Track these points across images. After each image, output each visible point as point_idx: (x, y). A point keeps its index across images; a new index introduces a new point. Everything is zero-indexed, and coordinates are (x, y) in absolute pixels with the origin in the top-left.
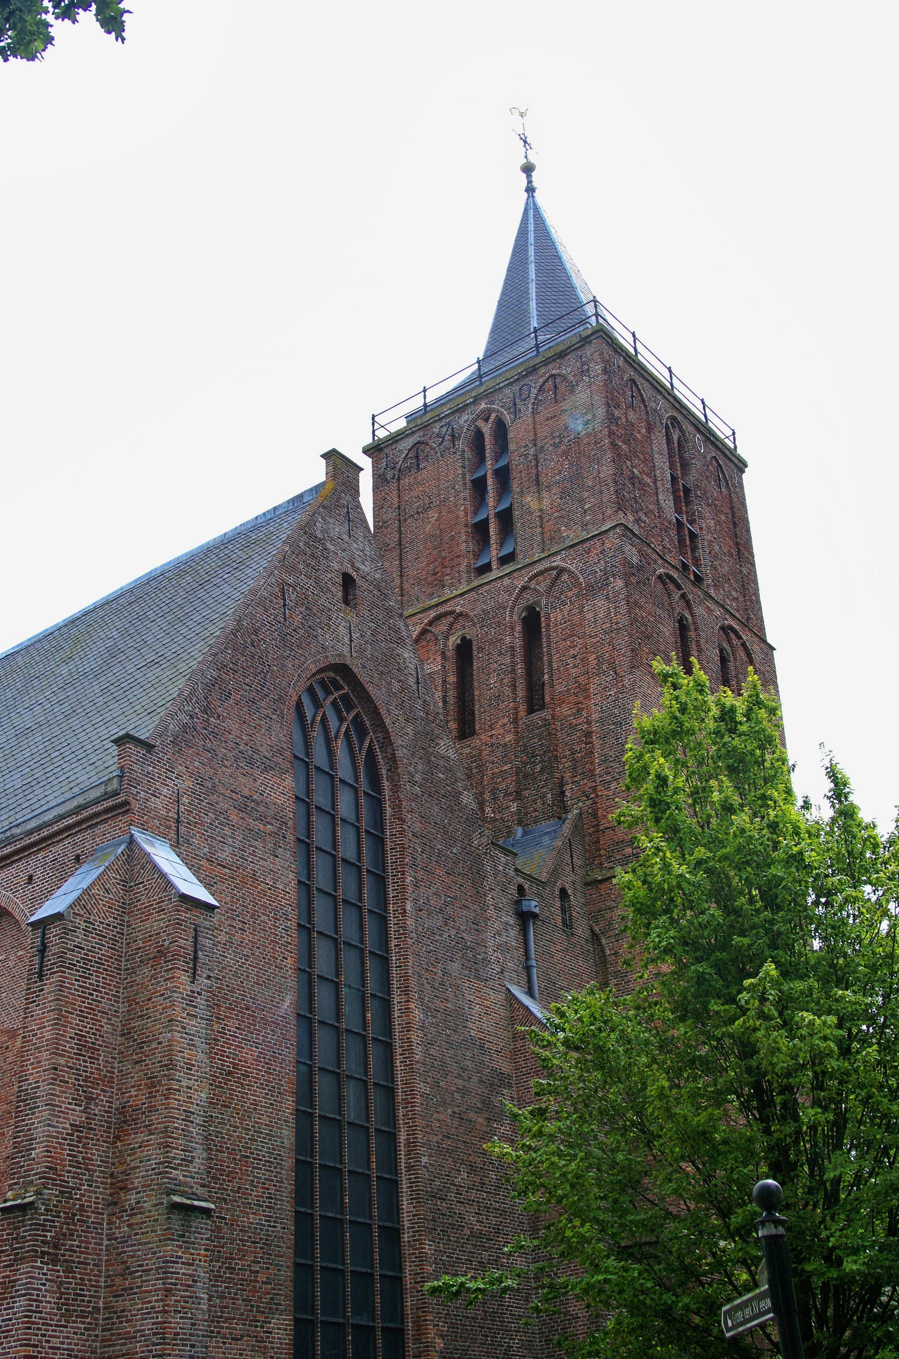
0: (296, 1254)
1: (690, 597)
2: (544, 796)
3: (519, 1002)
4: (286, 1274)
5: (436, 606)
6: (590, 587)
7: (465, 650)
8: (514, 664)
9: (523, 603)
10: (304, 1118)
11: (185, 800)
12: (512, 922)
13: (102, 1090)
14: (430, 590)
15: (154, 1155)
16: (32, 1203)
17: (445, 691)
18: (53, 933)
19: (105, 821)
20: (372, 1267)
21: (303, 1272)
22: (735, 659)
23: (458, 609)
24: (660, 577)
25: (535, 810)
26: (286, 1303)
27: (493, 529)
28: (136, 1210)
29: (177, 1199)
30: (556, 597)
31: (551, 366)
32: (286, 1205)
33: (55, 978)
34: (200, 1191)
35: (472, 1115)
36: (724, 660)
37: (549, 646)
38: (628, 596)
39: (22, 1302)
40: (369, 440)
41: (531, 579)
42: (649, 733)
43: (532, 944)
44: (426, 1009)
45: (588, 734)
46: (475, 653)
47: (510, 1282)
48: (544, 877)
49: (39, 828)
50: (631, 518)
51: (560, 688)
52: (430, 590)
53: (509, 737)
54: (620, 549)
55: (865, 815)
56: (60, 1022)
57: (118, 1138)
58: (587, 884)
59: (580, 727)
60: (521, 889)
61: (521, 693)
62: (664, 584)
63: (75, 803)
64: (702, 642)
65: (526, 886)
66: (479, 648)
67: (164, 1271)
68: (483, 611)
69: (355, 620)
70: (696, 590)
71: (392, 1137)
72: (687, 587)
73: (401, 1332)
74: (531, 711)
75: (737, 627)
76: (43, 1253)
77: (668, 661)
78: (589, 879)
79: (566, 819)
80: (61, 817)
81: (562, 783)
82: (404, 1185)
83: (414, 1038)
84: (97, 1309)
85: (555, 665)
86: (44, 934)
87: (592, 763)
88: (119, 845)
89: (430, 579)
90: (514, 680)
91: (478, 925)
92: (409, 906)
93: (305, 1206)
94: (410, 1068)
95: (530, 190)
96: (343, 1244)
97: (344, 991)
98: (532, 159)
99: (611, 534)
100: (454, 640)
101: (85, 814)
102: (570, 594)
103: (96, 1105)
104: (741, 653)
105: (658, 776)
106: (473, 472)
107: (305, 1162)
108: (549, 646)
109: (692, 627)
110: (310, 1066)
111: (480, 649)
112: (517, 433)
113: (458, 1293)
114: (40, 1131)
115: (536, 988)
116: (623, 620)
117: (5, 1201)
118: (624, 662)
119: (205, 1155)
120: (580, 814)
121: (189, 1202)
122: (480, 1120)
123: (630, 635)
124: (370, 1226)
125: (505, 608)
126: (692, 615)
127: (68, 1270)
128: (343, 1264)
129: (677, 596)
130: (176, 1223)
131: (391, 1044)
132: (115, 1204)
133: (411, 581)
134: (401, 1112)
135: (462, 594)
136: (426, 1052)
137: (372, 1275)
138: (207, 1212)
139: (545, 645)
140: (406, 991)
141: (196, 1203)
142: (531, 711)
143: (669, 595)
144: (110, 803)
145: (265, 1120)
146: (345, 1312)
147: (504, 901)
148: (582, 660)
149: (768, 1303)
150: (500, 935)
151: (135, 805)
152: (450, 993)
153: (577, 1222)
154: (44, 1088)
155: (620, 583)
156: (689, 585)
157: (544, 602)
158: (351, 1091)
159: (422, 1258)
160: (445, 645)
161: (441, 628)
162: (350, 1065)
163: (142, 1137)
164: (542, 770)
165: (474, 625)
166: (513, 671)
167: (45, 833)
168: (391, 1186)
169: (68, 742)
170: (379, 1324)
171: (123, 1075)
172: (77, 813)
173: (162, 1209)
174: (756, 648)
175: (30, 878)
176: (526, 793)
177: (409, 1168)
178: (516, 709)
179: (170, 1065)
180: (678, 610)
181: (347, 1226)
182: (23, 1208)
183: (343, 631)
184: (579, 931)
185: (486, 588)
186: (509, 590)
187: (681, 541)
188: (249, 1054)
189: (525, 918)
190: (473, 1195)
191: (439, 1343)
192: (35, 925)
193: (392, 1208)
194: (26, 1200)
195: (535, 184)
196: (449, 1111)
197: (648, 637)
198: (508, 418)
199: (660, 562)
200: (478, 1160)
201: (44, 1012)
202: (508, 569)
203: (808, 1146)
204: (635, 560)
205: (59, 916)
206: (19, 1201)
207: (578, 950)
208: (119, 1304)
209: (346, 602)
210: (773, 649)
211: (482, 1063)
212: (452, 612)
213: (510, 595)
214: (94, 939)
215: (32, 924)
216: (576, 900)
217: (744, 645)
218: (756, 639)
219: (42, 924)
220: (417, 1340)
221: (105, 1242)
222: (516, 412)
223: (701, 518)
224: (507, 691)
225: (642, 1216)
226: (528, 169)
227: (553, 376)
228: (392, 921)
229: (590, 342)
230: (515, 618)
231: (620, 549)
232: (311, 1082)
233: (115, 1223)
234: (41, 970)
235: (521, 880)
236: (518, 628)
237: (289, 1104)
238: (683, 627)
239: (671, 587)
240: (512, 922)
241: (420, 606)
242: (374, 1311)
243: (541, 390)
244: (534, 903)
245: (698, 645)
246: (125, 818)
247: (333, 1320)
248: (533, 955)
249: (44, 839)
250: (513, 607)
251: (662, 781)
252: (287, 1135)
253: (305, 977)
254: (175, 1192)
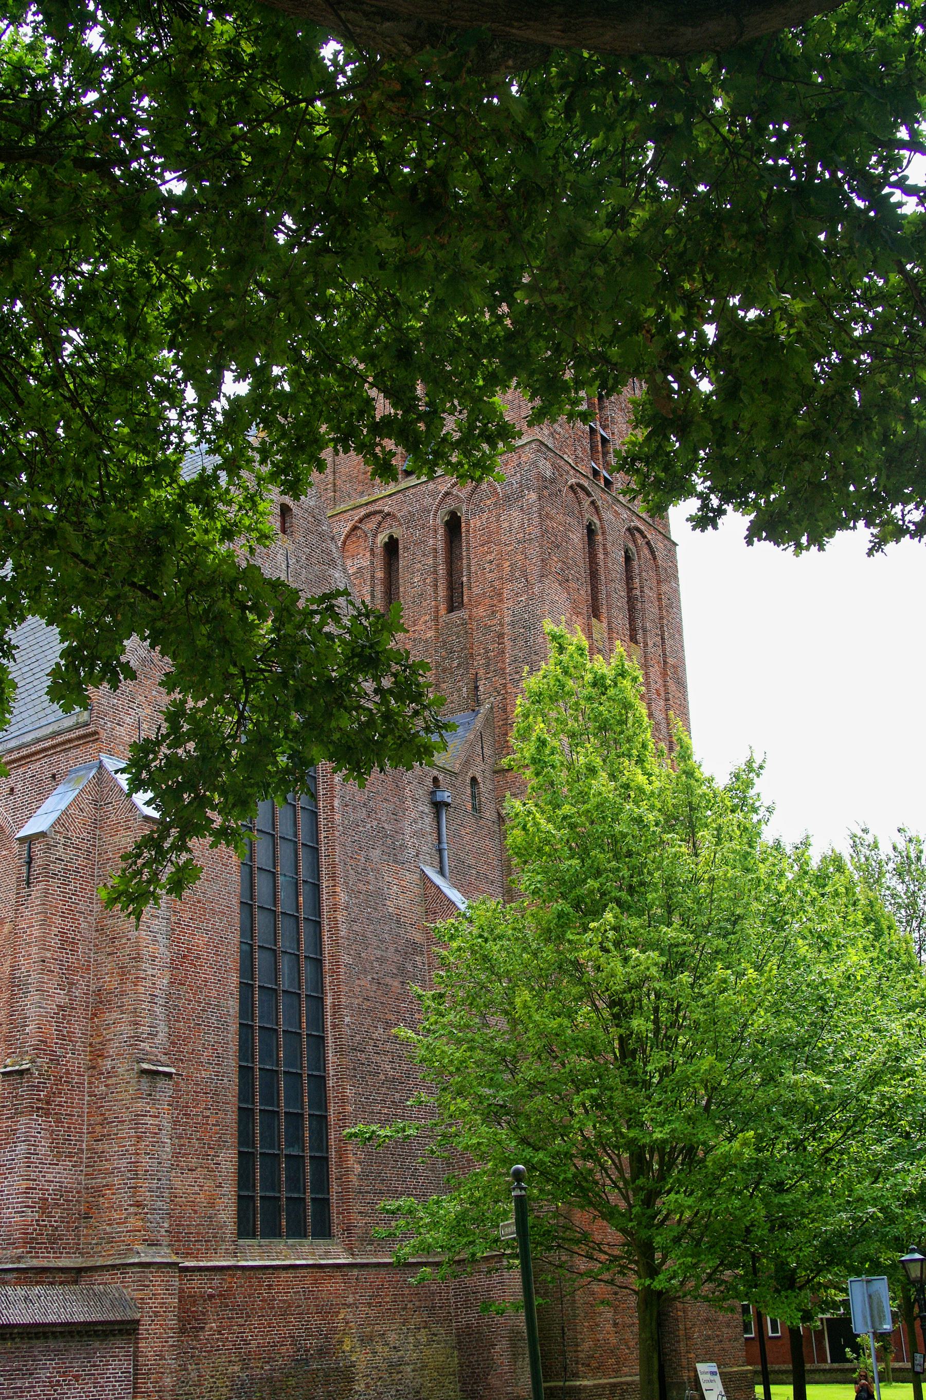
0: (240, 1101)
1: (599, 503)
2: (459, 690)
3: (431, 882)
4: (231, 1117)
5: (366, 504)
6: (507, 498)
7: (392, 547)
8: (436, 566)
9: (446, 508)
10: (246, 989)
11: (145, 726)
12: (427, 811)
13: (82, 977)
14: (360, 488)
15: (126, 1030)
16: (28, 1069)
17: (373, 587)
18: (38, 847)
19: (77, 746)
20: (302, 1109)
21: (245, 1115)
22: (639, 558)
23: (387, 509)
24: (571, 487)
25: (452, 702)
26: (231, 1139)
28: (110, 1074)
29: (145, 1066)
30: (476, 505)
32: (232, 1063)
33: (41, 886)
34: (163, 1058)
35: (388, 980)
36: (628, 559)
37: (468, 550)
38: (541, 508)
39: (22, 1147)
42: (535, 694)
43: (444, 830)
44: (350, 892)
45: (501, 635)
46: (401, 552)
47: (411, 1132)
48: (457, 768)
49: (19, 748)
50: (546, 432)
51: (476, 591)
52: (360, 488)
53: (431, 634)
54: (535, 464)
55: (705, 772)
56: (46, 922)
57: (95, 1015)
58: (495, 772)
59: (493, 628)
60: (435, 780)
61: (442, 592)
62: (575, 493)
63: (50, 729)
64: (609, 545)
65: (440, 778)
66: (404, 547)
67: (137, 1122)
69: (291, 547)
70: (605, 496)
71: (319, 1001)
72: (597, 494)
73: (326, 1159)
74: (451, 609)
75: (642, 528)
76: (38, 1108)
77: (557, 623)
78: (497, 768)
79: (478, 712)
80: (39, 740)
81: (476, 679)
82: (330, 1040)
83: (339, 918)
84: (82, 1150)
85: (473, 569)
86: (30, 848)
87: (504, 662)
88: (91, 769)
89: (361, 477)
90: (436, 580)
91: (396, 816)
92: (336, 803)
93: (247, 1061)
94: (336, 943)
96: (278, 1090)
97: (280, 879)
99: (527, 448)
100: (382, 538)
101: (60, 739)
102: (489, 502)
103: (77, 988)
104: (646, 552)
105: (539, 739)
107: (247, 1025)
108: (468, 550)
109: (600, 532)
110: (251, 945)
111: (406, 549)
113: (369, 1139)
114: (32, 1012)
115: (447, 868)
116: (536, 532)
117: (6, 1067)
118: (534, 571)
119: (167, 1030)
120: (492, 708)
121: (154, 1068)
122: (396, 984)
123: (541, 546)
124: (301, 1075)
125: (429, 511)
126: (600, 520)
127: (58, 1121)
128: (279, 1106)
129: (586, 503)
130: (145, 1083)
131: (319, 923)
132: (94, 1068)
133: (344, 478)
134: (328, 980)
135: (390, 495)
136: (350, 929)
137: (302, 1115)
138: (169, 1075)
139: (464, 549)
140: (333, 877)
141: (161, 1069)
142: (451, 609)
143: (580, 503)
144: (81, 732)
145: (214, 993)
146: (279, 1145)
147: (421, 792)
148: (497, 565)
149: (514, 1228)
150: (416, 823)
151: (103, 735)
152: (371, 876)
153: (459, 1100)
154: (34, 977)
155: (533, 496)
156: (599, 491)
157: (464, 508)
158: (285, 964)
159: (343, 1101)
160: (374, 543)
161: (370, 525)
162: (283, 943)
163: (115, 1015)
164: (459, 665)
165: (401, 525)
166: (435, 572)
167: (24, 752)
168: (319, 1041)
169: (37, 657)
170: (308, 1153)
171: (98, 964)
172: (52, 738)
173: (133, 1074)
174: (659, 545)
175: (12, 789)
176: (444, 686)
177: (334, 1026)
179: (138, 958)
180: (587, 516)
181: (282, 1076)
182: (21, 1073)
183: (280, 558)
184: (487, 815)
185: (412, 491)
186: (433, 494)
187: (593, 448)
188: (200, 940)
189: (438, 806)
190: (388, 1047)
191: (358, 1169)
192: (22, 840)
193: (319, 1060)
194: (24, 1067)
196: (369, 978)
197: (558, 547)
199: (572, 472)
200: (393, 1018)
201: (31, 916)
204: (548, 474)
205: (43, 834)
206: (17, 1068)
207: (485, 831)
208: (100, 1147)
209: (284, 531)
210: (675, 544)
211: (398, 935)
212: (380, 512)
214: (71, 852)
215: (18, 839)
216: (484, 787)
217: (648, 543)
218: (660, 537)
219: (29, 840)
220: (339, 1166)
221: (87, 1098)
223: (613, 422)
224: (430, 590)
225: (511, 1092)
228: (322, 816)
230: (438, 521)
231: (535, 464)
232: (252, 959)
233: (93, 1083)
234: (28, 879)
235: (435, 773)
236: (441, 531)
237: (234, 979)
238: (591, 531)
239: (582, 495)
240: (427, 811)
241: (352, 503)
242: (303, 1143)
244: (447, 794)
245: (605, 549)
246: (95, 746)
247: (271, 1151)
249: (28, 756)
250: (436, 511)
251: (543, 743)
252: (233, 1005)
253: (247, 869)
254: (143, 1060)
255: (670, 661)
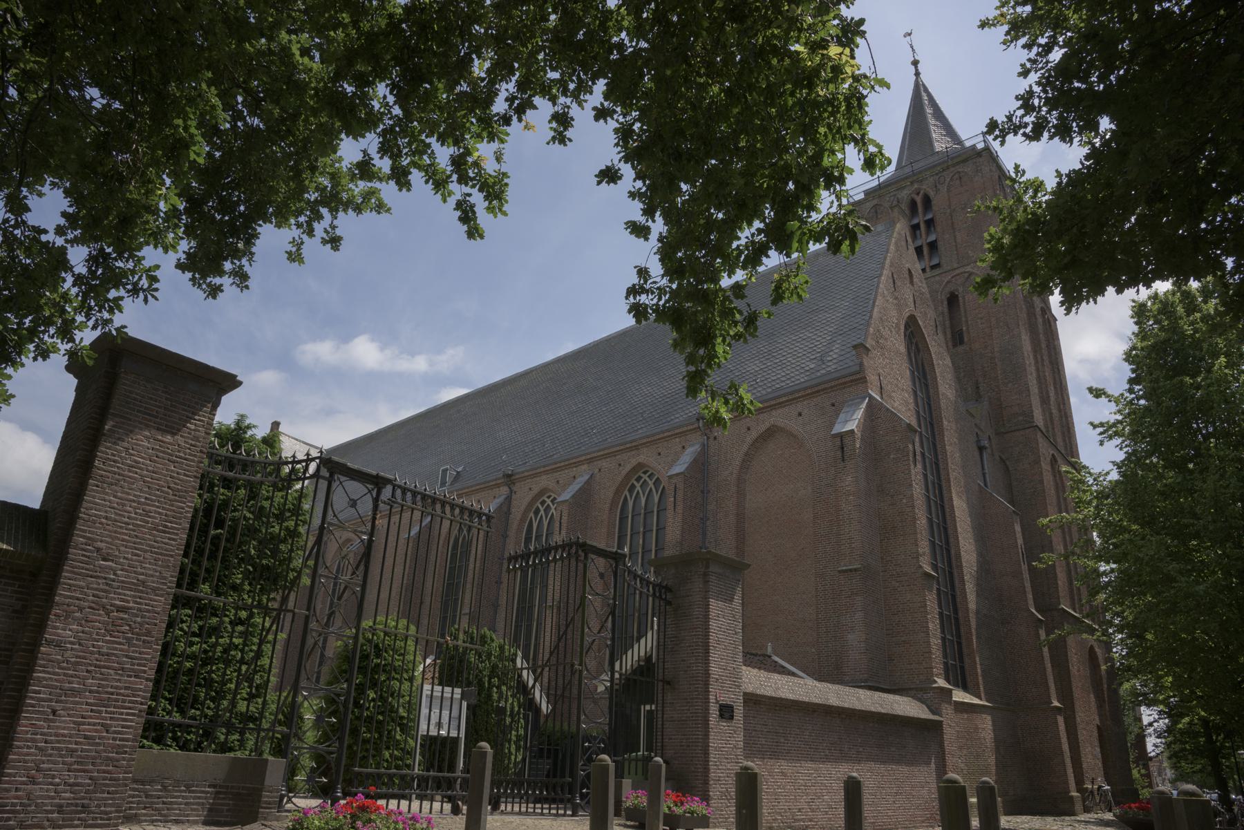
27: (926, 250)
95: (917, 74)
98: (917, 58)
106: (910, 220)
112: (937, 202)
195: (920, 70)
198: (932, 194)
202: (937, 271)
222: (937, 190)
226: (915, 63)
227: (959, 172)
230: (943, 297)
243: (952, 179)
248: (986, 467)
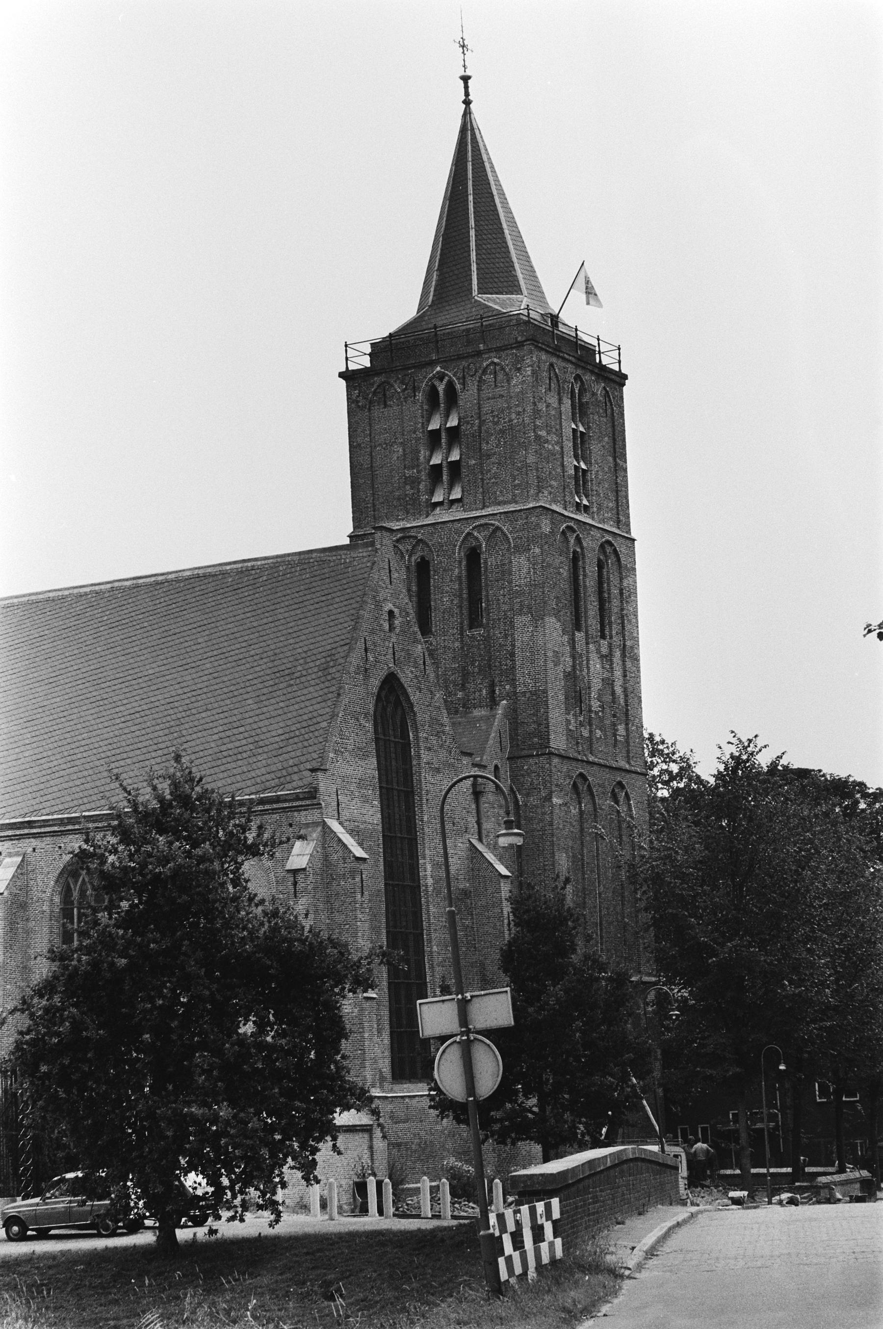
8: (461, 589)
18: (300, 877)
23: (420, 536)
25: (474, 699)
31: (492, 354)
40: (344, 369)
41: (474, 528)
68: (439, 543)
95: (467, 102)
102: (502, 547)
133: (381, 500)
166: (460, 596)
178: (461, 623)
203: (11, 1184)
213: (459, 536)
224: (456, 610)
226: (466, 79)
229: (524, 346)
230: (462, 554)
236: (464, 563)
255: (628, 643)
